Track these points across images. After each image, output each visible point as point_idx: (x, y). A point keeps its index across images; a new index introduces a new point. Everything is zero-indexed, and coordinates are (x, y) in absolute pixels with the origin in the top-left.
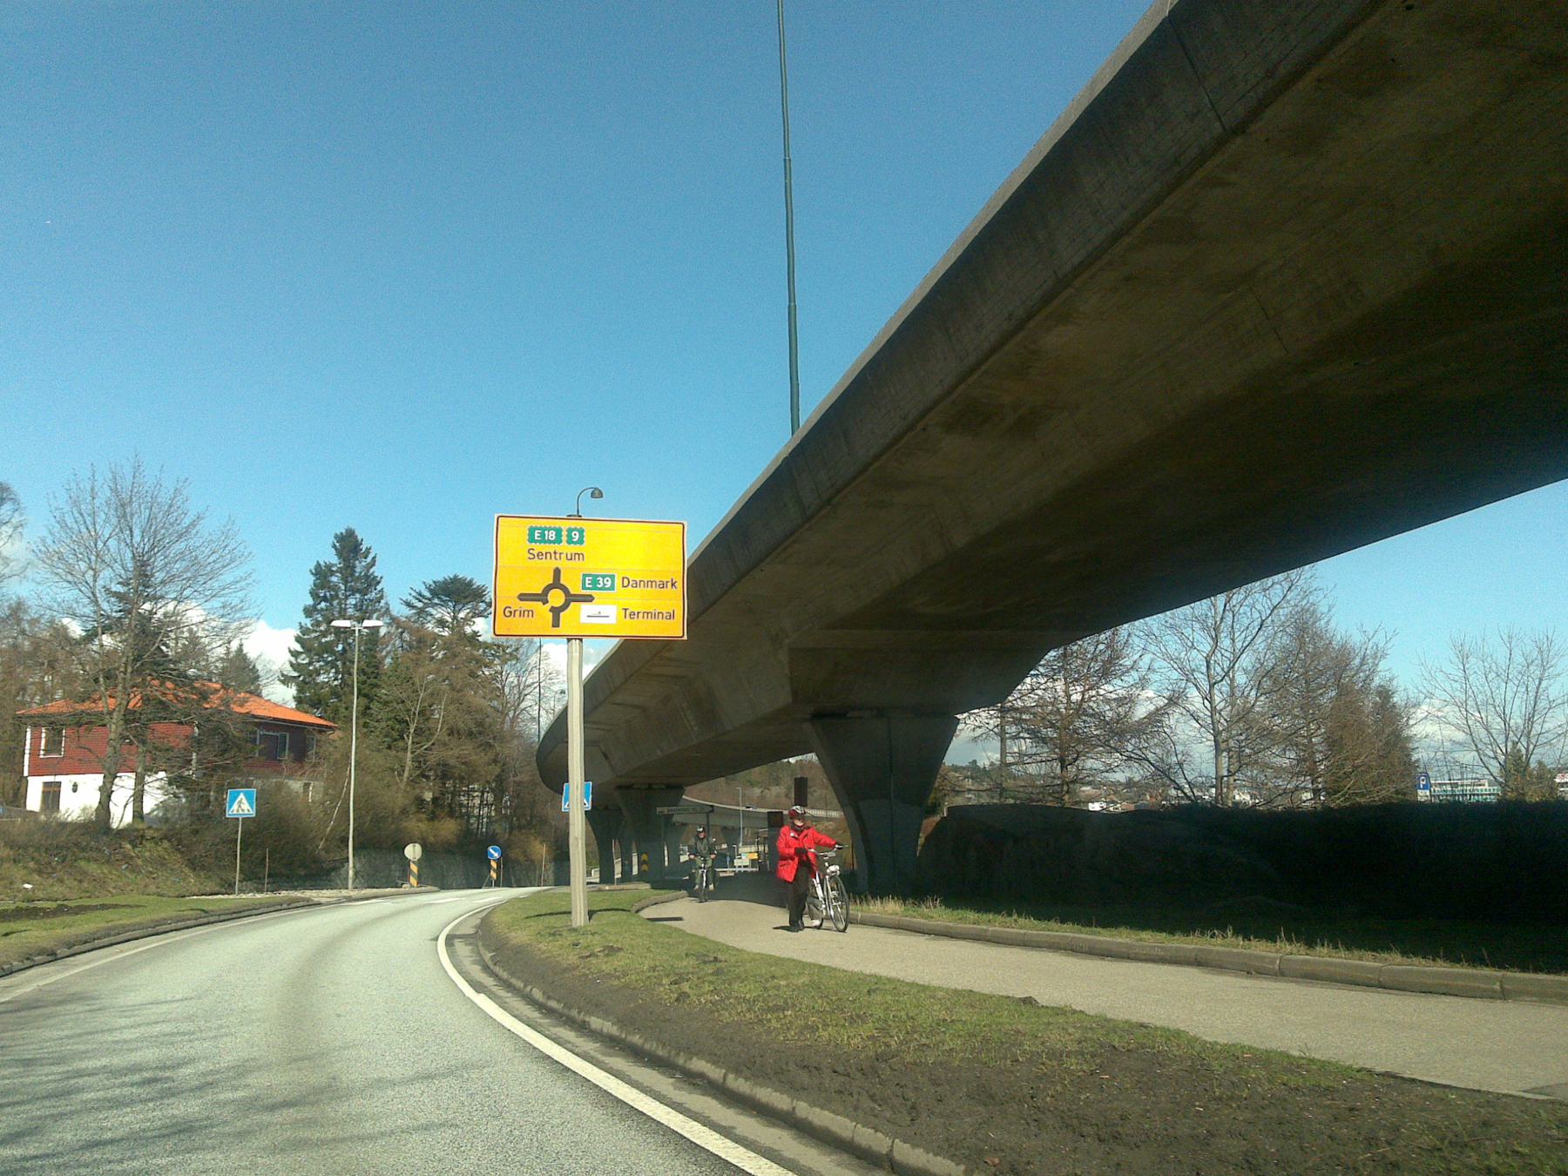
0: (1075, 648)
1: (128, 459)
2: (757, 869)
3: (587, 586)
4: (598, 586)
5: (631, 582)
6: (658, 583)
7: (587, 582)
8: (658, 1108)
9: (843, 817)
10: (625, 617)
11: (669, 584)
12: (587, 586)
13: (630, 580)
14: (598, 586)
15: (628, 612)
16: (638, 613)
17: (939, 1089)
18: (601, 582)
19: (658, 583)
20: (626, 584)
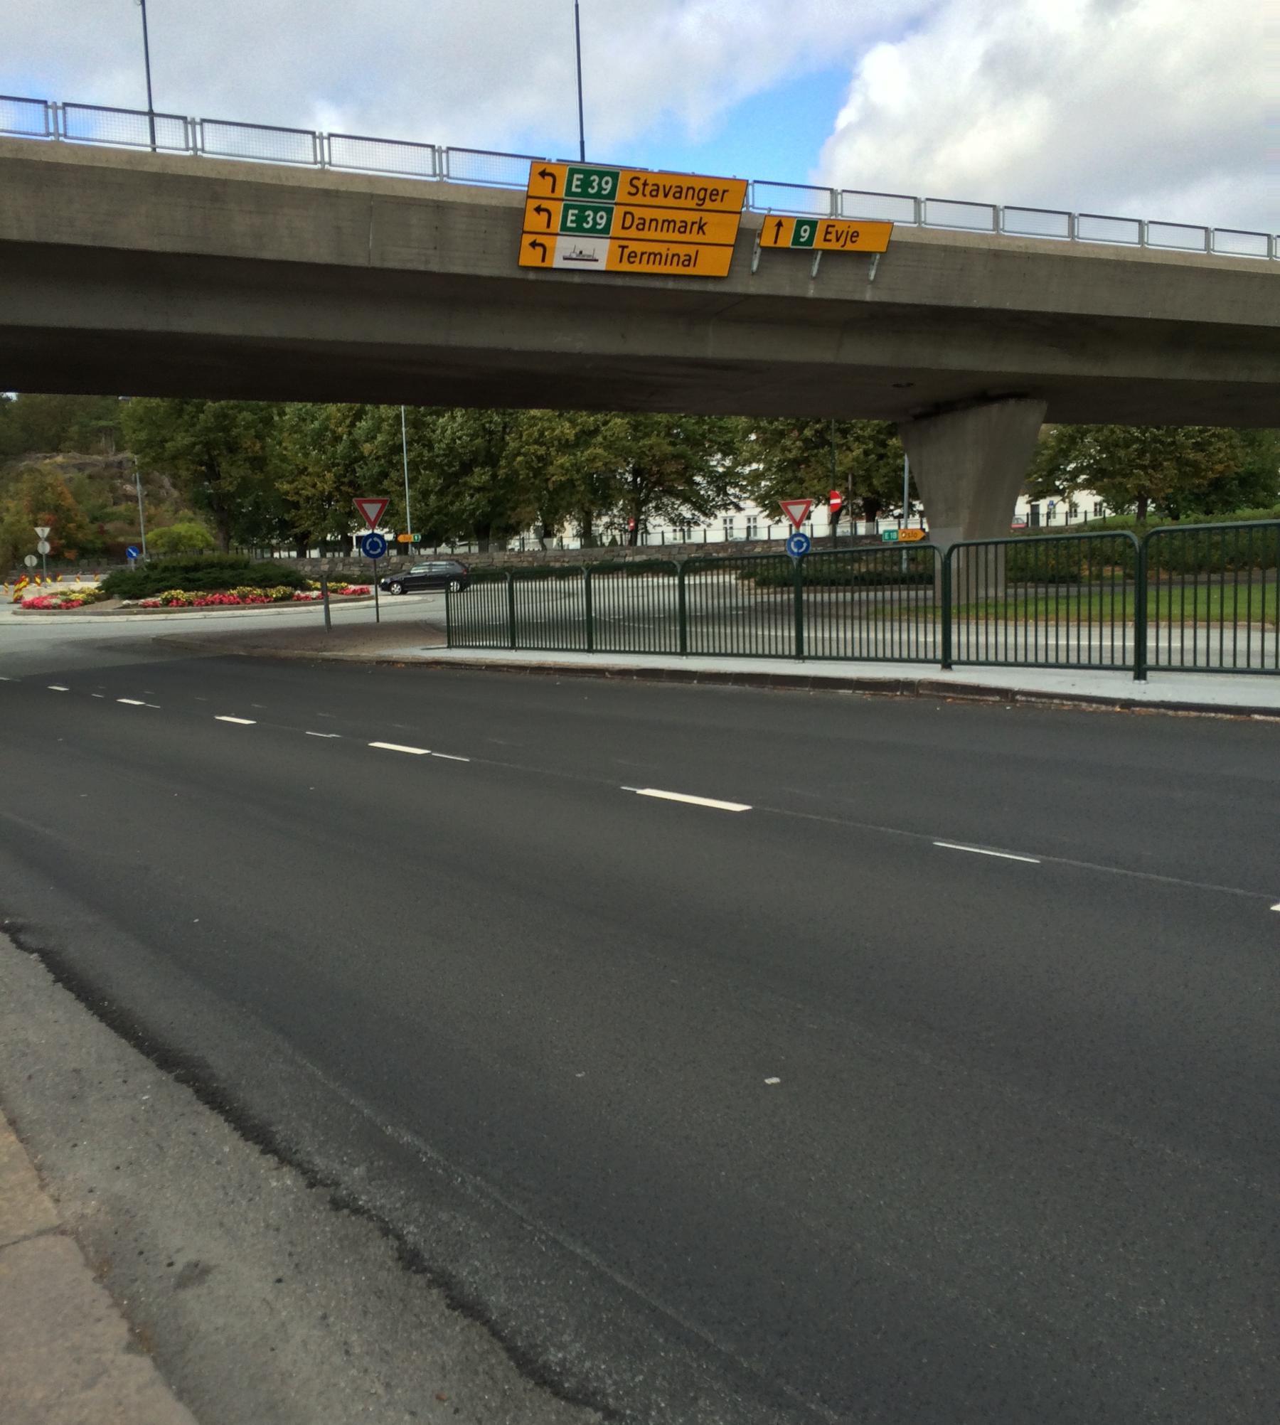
0: (871, 566)
1: (172, 1023)
2: (872, 442)
3: (574, 189)
4: (591, 191)
5: (636, 222)
6: (678, 225)
7: (575, 183)
8: (227, 131)
9: (879, 513)
10: (621, 261)
11: (696, 227)
12: (574, 189)
13: (636, 217)
14: (591, 191)
15: (627, 252)
16: (642, 254)
17: (270, 1297)
18: (590, 219)
19: (678, 225)
20: (627, 224)
